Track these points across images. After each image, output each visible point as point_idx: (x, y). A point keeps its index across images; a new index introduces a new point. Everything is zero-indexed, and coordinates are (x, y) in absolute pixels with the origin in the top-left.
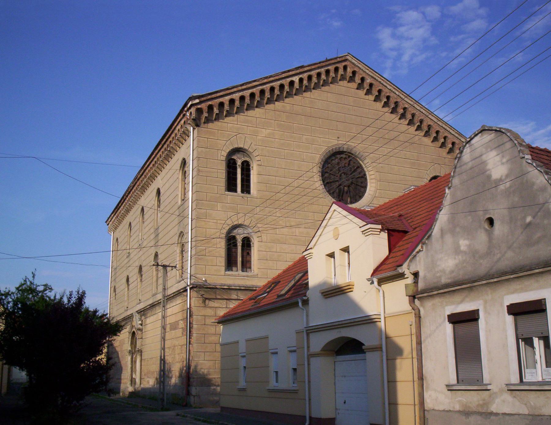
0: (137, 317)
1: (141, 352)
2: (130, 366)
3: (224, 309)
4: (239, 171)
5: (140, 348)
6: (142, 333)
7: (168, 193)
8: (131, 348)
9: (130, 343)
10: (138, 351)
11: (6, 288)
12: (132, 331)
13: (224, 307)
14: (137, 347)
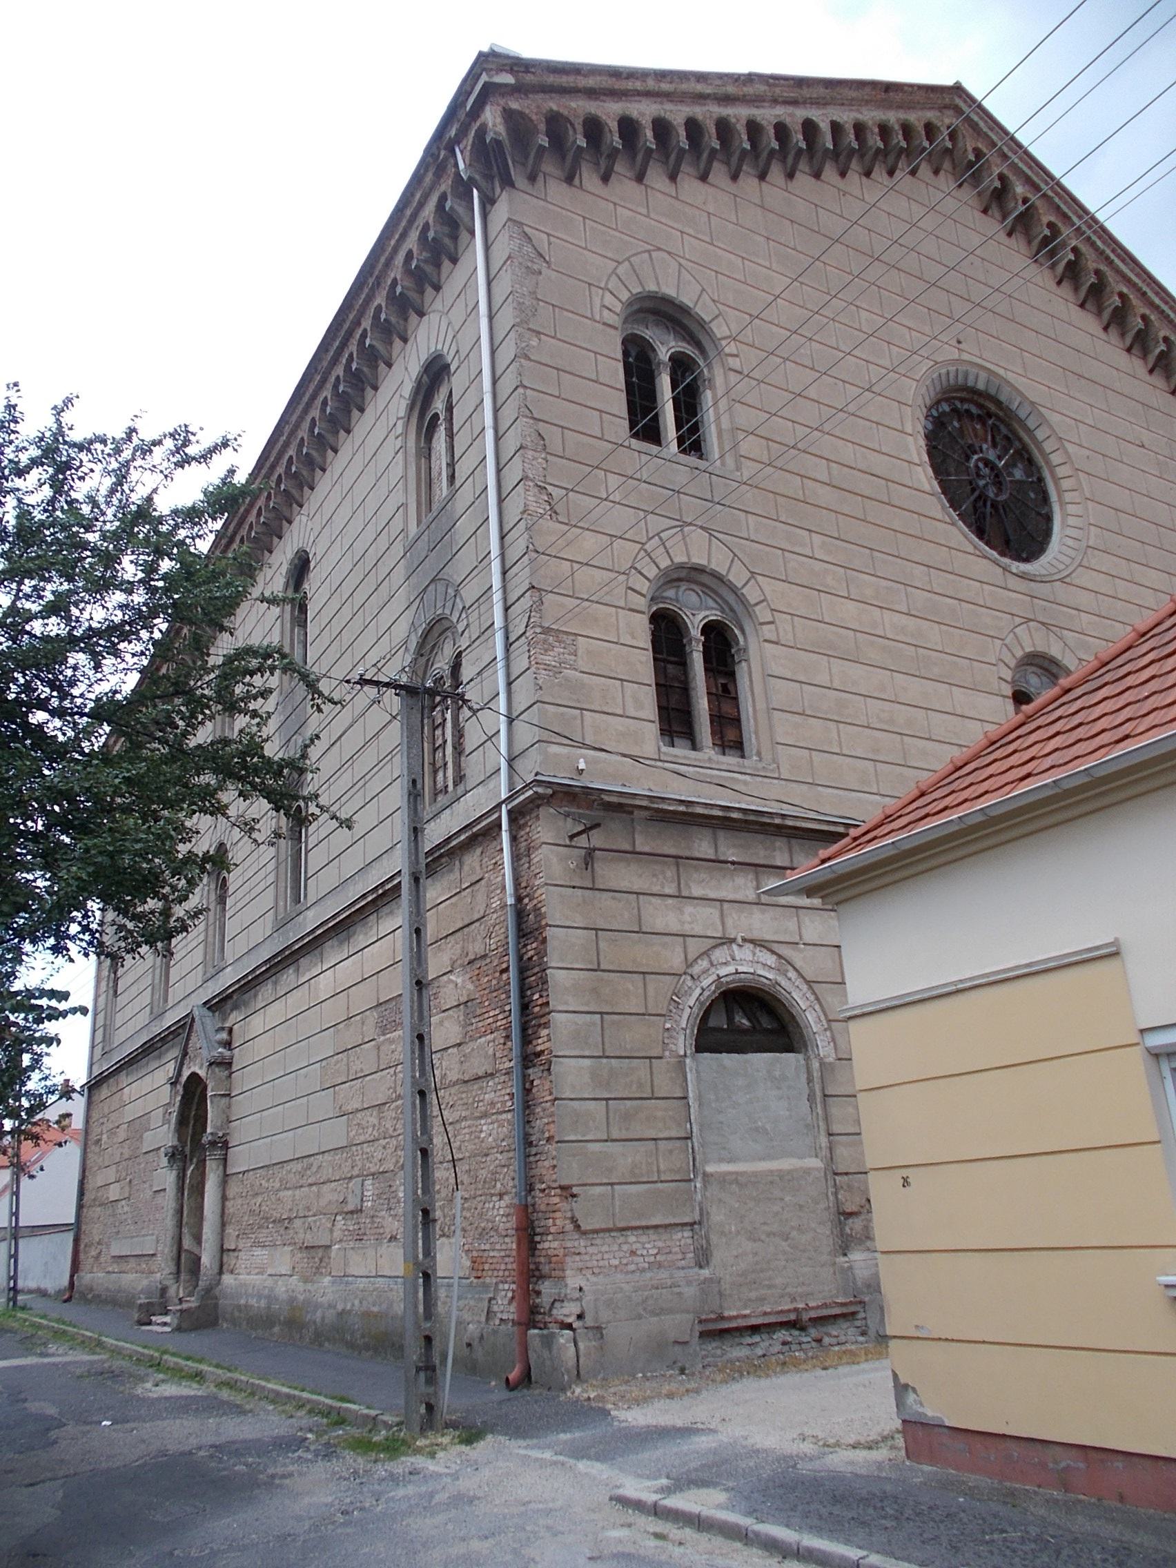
0: (207, 1025)
1: (226, 1146)
2: (712, 895)
3: (670, 901)
4: (665, 384)
5: (220, 1134)
6: (230, 1076)
7: (240, 894)
8: (179, 1139)
9: (173, 1121)
10: (213, 1144)
11: (42, 1169)
12: (186, 1074)
13: (667, 891)
14: (209, 1130)
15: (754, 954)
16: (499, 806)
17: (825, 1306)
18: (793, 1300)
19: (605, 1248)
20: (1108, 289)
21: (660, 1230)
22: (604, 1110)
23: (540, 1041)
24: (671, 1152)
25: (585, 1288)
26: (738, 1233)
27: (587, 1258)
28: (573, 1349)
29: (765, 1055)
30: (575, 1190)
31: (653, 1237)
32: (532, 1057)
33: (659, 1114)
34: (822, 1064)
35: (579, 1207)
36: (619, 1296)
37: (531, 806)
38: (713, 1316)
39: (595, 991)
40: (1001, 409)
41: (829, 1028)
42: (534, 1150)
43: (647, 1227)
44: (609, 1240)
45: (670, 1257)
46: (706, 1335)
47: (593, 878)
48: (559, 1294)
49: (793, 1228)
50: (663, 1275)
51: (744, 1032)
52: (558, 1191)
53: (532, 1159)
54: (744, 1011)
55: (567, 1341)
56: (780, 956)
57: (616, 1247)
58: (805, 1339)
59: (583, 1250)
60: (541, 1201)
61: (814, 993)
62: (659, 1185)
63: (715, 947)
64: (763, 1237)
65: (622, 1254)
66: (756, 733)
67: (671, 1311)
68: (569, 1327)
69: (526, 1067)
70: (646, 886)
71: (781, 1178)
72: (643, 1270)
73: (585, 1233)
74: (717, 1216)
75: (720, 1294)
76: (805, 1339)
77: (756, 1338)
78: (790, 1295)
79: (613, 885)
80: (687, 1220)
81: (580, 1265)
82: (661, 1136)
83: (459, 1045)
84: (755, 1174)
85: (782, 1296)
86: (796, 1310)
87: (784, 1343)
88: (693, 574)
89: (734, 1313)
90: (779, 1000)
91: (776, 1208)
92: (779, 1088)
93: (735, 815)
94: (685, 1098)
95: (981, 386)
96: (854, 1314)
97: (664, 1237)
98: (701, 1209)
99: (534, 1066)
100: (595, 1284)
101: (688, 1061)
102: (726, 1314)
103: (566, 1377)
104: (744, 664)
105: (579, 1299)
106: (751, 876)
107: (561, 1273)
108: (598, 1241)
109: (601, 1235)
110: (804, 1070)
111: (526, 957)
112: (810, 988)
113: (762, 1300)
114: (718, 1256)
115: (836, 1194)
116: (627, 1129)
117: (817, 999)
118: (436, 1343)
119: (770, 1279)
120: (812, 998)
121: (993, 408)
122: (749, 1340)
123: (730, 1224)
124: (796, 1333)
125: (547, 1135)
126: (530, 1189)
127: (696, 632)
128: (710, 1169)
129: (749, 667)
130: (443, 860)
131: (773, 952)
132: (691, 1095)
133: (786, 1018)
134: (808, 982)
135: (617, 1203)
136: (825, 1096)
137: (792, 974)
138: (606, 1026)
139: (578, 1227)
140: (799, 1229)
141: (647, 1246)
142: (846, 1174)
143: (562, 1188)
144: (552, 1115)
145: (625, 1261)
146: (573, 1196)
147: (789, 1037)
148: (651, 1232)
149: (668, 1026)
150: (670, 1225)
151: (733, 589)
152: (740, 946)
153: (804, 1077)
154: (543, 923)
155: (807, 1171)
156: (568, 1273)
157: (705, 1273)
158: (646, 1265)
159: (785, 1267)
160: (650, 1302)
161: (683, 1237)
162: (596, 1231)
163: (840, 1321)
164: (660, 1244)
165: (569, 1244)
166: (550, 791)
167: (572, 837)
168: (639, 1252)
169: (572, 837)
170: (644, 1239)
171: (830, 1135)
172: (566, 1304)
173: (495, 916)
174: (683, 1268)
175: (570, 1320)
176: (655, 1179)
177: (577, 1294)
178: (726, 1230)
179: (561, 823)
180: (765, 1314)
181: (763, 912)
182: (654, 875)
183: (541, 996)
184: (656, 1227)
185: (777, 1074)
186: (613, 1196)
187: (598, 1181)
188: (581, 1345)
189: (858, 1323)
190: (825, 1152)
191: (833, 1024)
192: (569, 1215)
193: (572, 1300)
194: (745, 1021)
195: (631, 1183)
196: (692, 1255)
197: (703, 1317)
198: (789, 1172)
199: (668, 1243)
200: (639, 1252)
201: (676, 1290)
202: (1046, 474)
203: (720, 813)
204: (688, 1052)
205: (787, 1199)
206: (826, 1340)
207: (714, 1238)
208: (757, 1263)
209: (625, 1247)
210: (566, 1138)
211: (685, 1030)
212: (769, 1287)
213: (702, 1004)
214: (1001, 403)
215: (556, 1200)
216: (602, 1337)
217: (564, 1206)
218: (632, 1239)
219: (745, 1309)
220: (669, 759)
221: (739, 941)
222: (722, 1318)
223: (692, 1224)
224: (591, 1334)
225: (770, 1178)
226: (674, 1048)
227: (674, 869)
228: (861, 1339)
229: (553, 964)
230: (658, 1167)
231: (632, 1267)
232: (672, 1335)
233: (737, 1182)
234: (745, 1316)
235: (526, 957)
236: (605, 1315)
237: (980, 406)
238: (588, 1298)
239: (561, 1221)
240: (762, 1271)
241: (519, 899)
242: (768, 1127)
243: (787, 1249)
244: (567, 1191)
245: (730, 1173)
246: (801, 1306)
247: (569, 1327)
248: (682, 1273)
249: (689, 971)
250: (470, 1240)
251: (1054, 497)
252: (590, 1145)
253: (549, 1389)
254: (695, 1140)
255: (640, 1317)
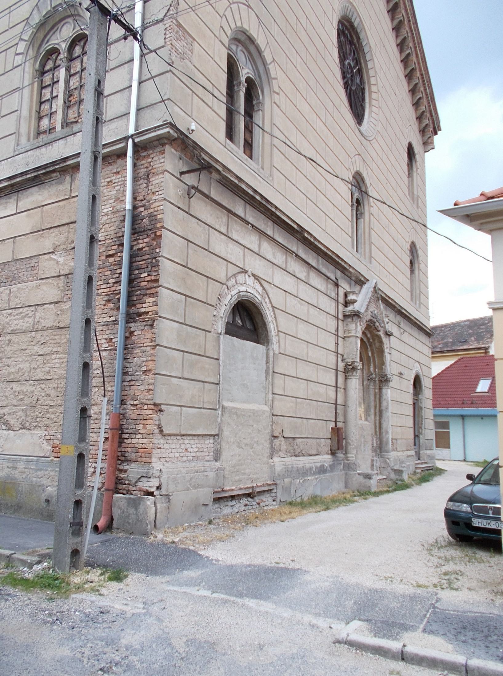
15: (254, 283)
16: (126, 139)
17: (264, 485)
18: (252, 482)
19: (173, 446)
20: (399, 10)
21: (200, 438)
22: (182, 356)
23: (144, 305)
24: (210, 390)
25: (163, 470)
26: (234, 443)
27: (163, 451)
28: (154, 508)
29: (251, 343)
30: (163, 407)
31: (196, 441)
32: (135, 316)
33: (207, 366)
34: (274, 354)
35: (163, 417)
36: (179, 475)
37: (156, 143)
38: (220, 490)
39: (183, 279)
40: (358, 42)
41: (278, 335)
42: (129, 378)
43: (194, 435)
44: (175, 441)
45: (203, 454)
46: (217, 500)
47: (189, 206)
48: (147, 473)
49: (255, 442)
50: (200, 464)
51: (239, 327)
52: (152, 407)
53: (125, 384)
54: (240, 316)
55: (151, 504)
56: (264, 289)
57: (178, 446)
58: (254, 503)
59: (162, 446)
60: (131, 412)
61: (274, 314)
62: (202, 410)
63: (238, 273)
64: (243, 446)
65: (181, 450)
66: (262, 157)
67: (201, 486)
68: (151, 494)
69: (127, 322)
70: (213, 223)
71: (254, 414)
72: (189, 461)
73: (164, 436)
74: (226, 433)
75: (224, 477)
76: (254, 503)
77: (234, 503)
78: (251, 479)
79: (198, 215)
80: (213, 433)
81: (160, 455)
82: (207, 380)
83: (56, 303)
84: (244, 410)
85: (248, 480)
86: (253, 487)
87: (246, 505)
88: (247, 42)
89: (228, 488)
90: (261, 314)
91: (250, 431)
92: (255, 364)
93: (258, 198)
94: (218, 359)
95: (356, 24)
96: (271, 490)
97: (202, 441)
98: (219, 427)
99: (135, 322)
100: (168, 468)
101: (222, 337)
102: (225, 489)
103: (149, 526)
104: (260, 112)
105: (159, 477)
106: (257, 238)
107: (148, 460)
108: (170, 441)
109: (172, 437)
110: (265, 356)
111: (135, 248)
112: (273, 310)
113: (240, 481)
114: (225, 455)
115: (272, 425)
116: (191, 373)
117: (275, 317)
118: (84, 506)
119: (244, 469)
120: (273, 316)
121: (355, 41)
122: (230, 503)
123: (231, 437)
124: (250, 499)
125: (144, 368)
126: (123, 402)
127: (243, 79)
128: (226, 404)
129: (263, 115)
130: (55, 174)
131: (262, 285)
132: (221, 358)
133: (260, 324)
134: (273, 307)
135: (183, 418)
136: (274, 372)
137: (267, 300)
138: (187, 304)
139: (161, 431)
140: (257, 443)
141: (193, 446)
142: (276, 415)
143: (155, 404)
144: (152, 355)
145: (182, 455)
146: (161, 411)
147: (257, 336)
148: (196, 438)
149: (215, 313)
150: (206, 435)
151: (265, 64)
152: (249, 276)
153: (265, 359)
154: (159, 225)
155: (264, 412)
156: (154, 460)
157: (218, 464)
158: (191, 458)
159: (250, 463)
160: (193, 480)
161: (209, 442)
162: (170, 435)
163: (266, 493)
164: (199, 446)
165: (155, 442)
166: (176, 135)
167: (182, 173)
168: (189, 450)
169: (182, 173)
170: (192, 442)
171: (273, 394)
172: (151, 480)
173: (106, 218)
174: (208, 461)
175: (152, 490)
176: (201, 406)
177: (158, 474)
178: (229, 441)
179: (177, 161)
180: (241, 489)
181: (260, 261)
182: (218, 218)
183: (149, 275)
184: (198, 435)
185: (255, 355)
186: (181, 413)
187: (174, 403)
188: (158, 506)
189: (273, 495)
190: (270, 403)
191: (280, 333)
192: (157, 423)
193: (155, 477)
194: (239, 322)
195: (190, 407)
196: (212, 454)
197: (216, 490)
198: (257, 411)
199: (203, 446)
200: (189, 450)
201: (205, 473)
202: (366, 87)
203: (251, 193)
204: (223, 332)
205: (254, 426)
206: (262, 504)
207: (224, 445)
208: (240, 460)
209: (183, 446)
210: (161, 373)
211: (222, 318)
212: (244, 474)
213: (231, 305)
214: (360, 39)
215: (150, 412)
216: (169, 500)
217: (155, 416)
218: (186, 441)
219: (233, 486)
220: (230, 149)
221: (249, 273)
222: (223, 491)
223: (214, 436)
224: (163, 498)
225: (249, 414)
226: (216, 328)
227: (226, 217)
228: (274, 503)
229: (164, 255)
230: (203, 399)
231: (185, 459)
232: (202, 501)
233: (236, 413)
234: (232, 490)
235: (135, 248)
236: (172, 488)
237: (351, 36)
238: (164, 477)
239: (152, 427)
240: (242, 465)
241: (135, 208)
242: (248, 384)
243: (252, 453)
244: (158, 408)
245: (234, 408)
246: (255, 485)
247: (151, 494)
248: (207, 464)
249: (227, 284)
250: (52, 433)
251: (367, 100)
252: (173, 379)
253: (132, 533)
254: (220, 386)
255: (188, 489)
